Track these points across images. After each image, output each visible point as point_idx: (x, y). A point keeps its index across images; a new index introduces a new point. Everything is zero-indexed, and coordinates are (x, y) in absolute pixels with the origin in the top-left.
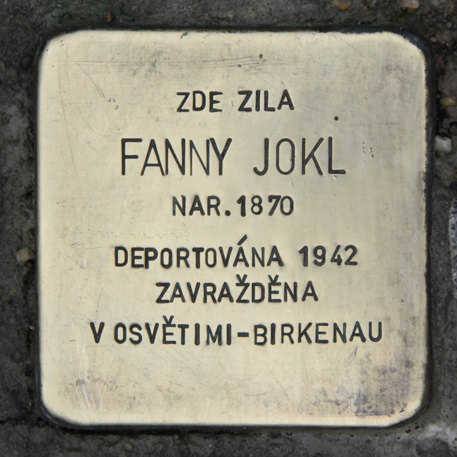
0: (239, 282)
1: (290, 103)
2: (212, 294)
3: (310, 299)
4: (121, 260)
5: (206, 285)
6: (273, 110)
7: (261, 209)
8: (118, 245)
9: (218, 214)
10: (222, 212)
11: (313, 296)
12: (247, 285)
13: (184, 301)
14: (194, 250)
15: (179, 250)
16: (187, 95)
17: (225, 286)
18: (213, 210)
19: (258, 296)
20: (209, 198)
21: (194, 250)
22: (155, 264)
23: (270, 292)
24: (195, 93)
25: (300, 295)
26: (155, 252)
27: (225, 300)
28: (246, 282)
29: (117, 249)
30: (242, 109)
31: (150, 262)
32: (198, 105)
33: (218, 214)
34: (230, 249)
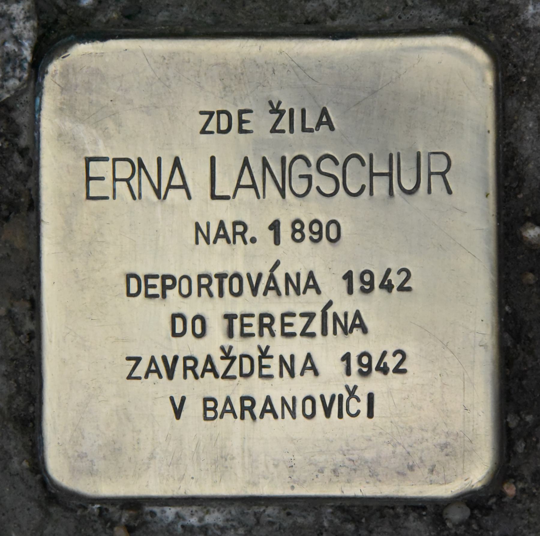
0: (223, 355)
1: (329, 123)
2: (193, 369)
4: (134, 289)
5: (186, 359)
6: (311, 130)
10: (248, 239)
11: (313, 371)
12: (233, 359)
13: (160, 376)
14: (217, 276)
15: (200, 277)
16: (211, 114)
17: (209, 359)
19: (247, 369)
22: (173, 294)
23: (261, 367)
24: (219, 113)
25: (298, 369)
26: (173, 278)
28: (231, 355)
29: (129, 276)
30: (273, 130)
31: (168, 292)
34: (260, 276)
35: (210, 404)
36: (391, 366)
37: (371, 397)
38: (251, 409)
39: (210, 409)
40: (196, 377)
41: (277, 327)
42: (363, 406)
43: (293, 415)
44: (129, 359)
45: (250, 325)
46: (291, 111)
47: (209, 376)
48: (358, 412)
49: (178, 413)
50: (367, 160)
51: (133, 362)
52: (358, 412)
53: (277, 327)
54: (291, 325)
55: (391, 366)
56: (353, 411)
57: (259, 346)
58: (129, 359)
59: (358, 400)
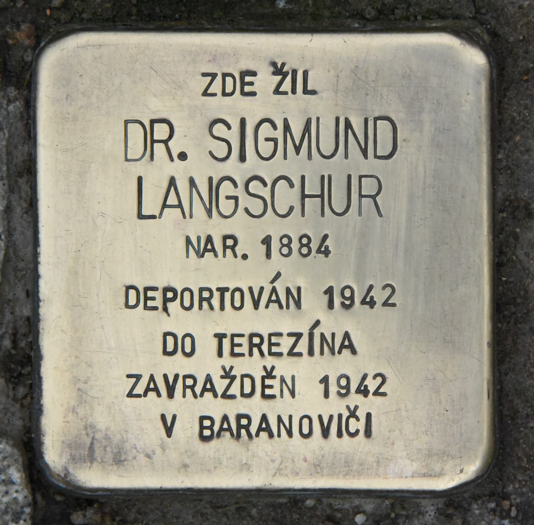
0: (224, 374)
2: (192, 388)
3: (346, 352)
4: (132, 301)
5: (185, 377)
7: (290, 249)
8: (129, 283)
9: (235, 256)
10: (239, 254)
11: (350, 349)
14: (218, 289)
15: (201, 290)
17: (208, 379)
18: (229, 251)
20: (225, 238)
21: (218, 289)
23: (264, 387)
24: (225, 75)
27: (208, 395)
28: (233, 373)
29: (129, 288)
31: (170, 305)
32: (229, 89)
33: (235, 256)
34: (262, 289)
35: (207, 423)
36: (372, 389)
37: (369, 416)
38: (247, 428)
39: (207, 428)
40: (195, 396)
41: (265, 348)
42: (361, 425)
43: (290, 433)
44: (129, 376)
45: (240, 345)
46: (295, 72)
47: (208, 395)
48: (357, 431)
49: (169, 431)
50: (297, 182)
51: (134, 380)
52: (357, 431)
53: (265, 348)
54: (278, 345)
55: (372, 389)
56: (352, 430)
57: (223, 367)
58: (129, 376)
59: (358, 419)
